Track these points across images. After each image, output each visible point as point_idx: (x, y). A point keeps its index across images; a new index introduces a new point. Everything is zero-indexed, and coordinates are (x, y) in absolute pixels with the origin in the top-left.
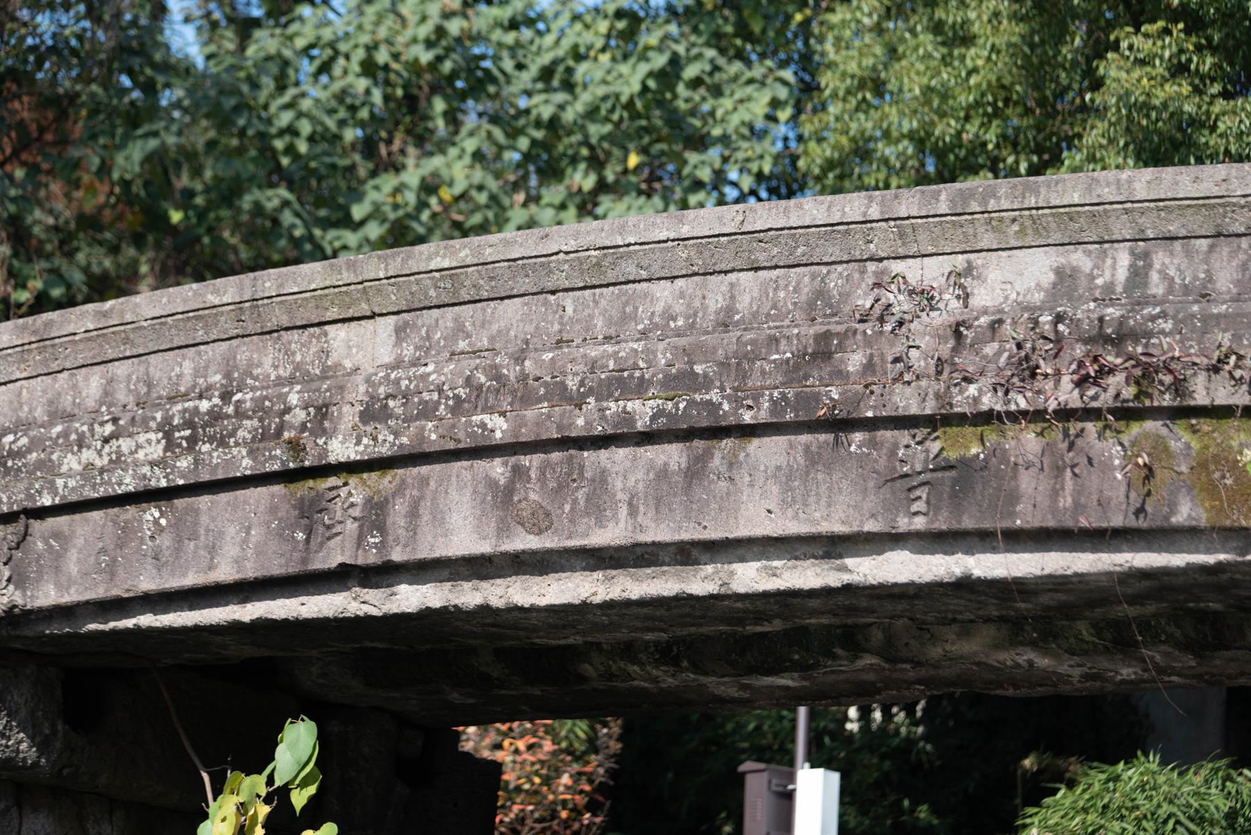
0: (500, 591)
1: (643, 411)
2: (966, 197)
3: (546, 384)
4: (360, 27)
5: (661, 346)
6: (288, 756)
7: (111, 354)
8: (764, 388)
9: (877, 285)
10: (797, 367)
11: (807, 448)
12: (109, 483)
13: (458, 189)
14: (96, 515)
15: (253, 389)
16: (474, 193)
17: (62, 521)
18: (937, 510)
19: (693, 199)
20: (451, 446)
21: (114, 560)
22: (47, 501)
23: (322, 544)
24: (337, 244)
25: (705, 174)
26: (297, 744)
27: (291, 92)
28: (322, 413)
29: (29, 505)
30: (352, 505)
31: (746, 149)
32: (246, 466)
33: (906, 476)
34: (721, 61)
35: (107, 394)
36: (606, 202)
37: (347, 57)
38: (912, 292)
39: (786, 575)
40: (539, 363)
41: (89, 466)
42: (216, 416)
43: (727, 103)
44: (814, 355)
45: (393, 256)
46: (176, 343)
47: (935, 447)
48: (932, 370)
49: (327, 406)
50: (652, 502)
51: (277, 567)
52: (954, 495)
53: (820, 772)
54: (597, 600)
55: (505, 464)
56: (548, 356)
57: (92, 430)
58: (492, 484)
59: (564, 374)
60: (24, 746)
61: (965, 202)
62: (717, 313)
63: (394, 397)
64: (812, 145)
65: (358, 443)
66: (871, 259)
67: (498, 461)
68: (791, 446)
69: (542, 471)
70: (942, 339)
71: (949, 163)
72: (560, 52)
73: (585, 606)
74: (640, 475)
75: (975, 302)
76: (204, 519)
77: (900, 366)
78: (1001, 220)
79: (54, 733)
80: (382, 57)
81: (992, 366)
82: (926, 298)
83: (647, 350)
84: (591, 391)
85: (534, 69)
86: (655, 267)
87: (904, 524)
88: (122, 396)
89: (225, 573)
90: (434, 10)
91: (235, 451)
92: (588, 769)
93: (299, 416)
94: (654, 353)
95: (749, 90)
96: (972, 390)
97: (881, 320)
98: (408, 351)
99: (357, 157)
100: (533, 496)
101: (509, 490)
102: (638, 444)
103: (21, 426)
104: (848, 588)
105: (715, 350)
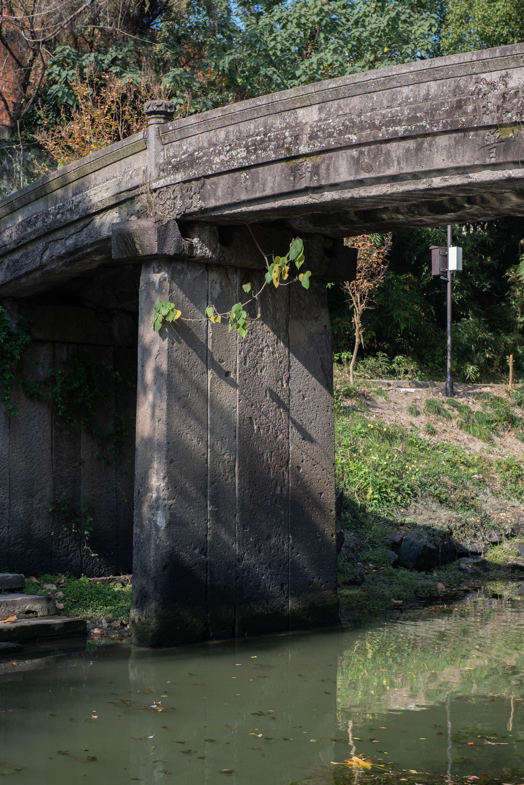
0: (357, 192)
1: (401, 130)
2: (505, 50)
3: (369, 123)
4: (295, 12)
5: (406, 108)
6: (294, 250)
7: (227, 123)
8: (440, 119)
9: (476, 82)
10: (451, 112)
11: (455, 138)
12: (230, 165)
13: (329, 63)
14: (226, 176)
15: (274, 132)
16: (334, 62)
17: (215, 179)
18: (499, 156)
19: (406, 60)
20: (339, 146)
21: (233, 190)
22: (210, 172)
23: (299, 181)
24: (292, 85)
25: (409, 51)
26: (297, 247)
27: (274, 35)
28: (297, 138)
29: (204, 174)
30: (308, 167)
31: (422, 42)
32: (273, 157)
33: (488, 145)
34: (412, 14)
35: (227, 136)
36: (377, 64)
37: (292, 22)
38: (488, 84)
39: (450, 180)
40: (366, 117)
41: (223, 160)
42: (262, 141)
43: (416, 27)
44: (456, 108)
45: (317, 85)
46: (248, 118)
47: (498, 135)
48: (496, 109)
49: (298, 136)
50: (405, 160)
51: (285, 189)
52: (504, 150)
53: (455, 248)
54: (389, 193)
55: (357, 151)
56: (369, 114)
57: (223, 149)
58: (353, 157)
59: (374, 119)
60: (208, 252)
61: (505, 52)
62: (423, 96)
63: (319, 131)
64: (444, 39)
65: (309, 147)
66: (474, 74)
67: (354, 150)
68: (450, 138)
69: (369, 152)
70: (498, 99)
71: (489, 41)
72: (360, 15)
73: (385, 195)
74: (401, 151)
75: (509, 86)
76: (261, 175)
77: (485, 109)
78: (517, 57)
79: (217, 247)
80: (303, 20)
81: (516, 107)
82: (492, 85)
83: (401, 110)
84: (383, 125)
85: (352, 21)
86: (403, 82)
87: (488, 161)
88: (232, 137)
89: (268, 192)
90: (319, 3)
91: (269, 152)
92: (382, 251)
93: (289, 139)
94: (404, 110)
95: (422, 22)
96: (509, 115)
97: (478, 94)
98: (323, 116)
99: (296, 56)
100: (366, 160)
101: (358, 159)
102: (399, 141)
103: (200, 149)
104: (470, 184)
105: (423, 108)
